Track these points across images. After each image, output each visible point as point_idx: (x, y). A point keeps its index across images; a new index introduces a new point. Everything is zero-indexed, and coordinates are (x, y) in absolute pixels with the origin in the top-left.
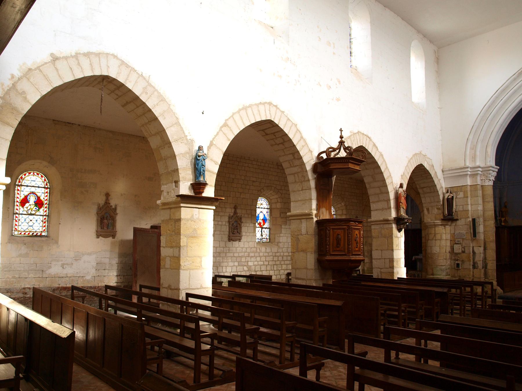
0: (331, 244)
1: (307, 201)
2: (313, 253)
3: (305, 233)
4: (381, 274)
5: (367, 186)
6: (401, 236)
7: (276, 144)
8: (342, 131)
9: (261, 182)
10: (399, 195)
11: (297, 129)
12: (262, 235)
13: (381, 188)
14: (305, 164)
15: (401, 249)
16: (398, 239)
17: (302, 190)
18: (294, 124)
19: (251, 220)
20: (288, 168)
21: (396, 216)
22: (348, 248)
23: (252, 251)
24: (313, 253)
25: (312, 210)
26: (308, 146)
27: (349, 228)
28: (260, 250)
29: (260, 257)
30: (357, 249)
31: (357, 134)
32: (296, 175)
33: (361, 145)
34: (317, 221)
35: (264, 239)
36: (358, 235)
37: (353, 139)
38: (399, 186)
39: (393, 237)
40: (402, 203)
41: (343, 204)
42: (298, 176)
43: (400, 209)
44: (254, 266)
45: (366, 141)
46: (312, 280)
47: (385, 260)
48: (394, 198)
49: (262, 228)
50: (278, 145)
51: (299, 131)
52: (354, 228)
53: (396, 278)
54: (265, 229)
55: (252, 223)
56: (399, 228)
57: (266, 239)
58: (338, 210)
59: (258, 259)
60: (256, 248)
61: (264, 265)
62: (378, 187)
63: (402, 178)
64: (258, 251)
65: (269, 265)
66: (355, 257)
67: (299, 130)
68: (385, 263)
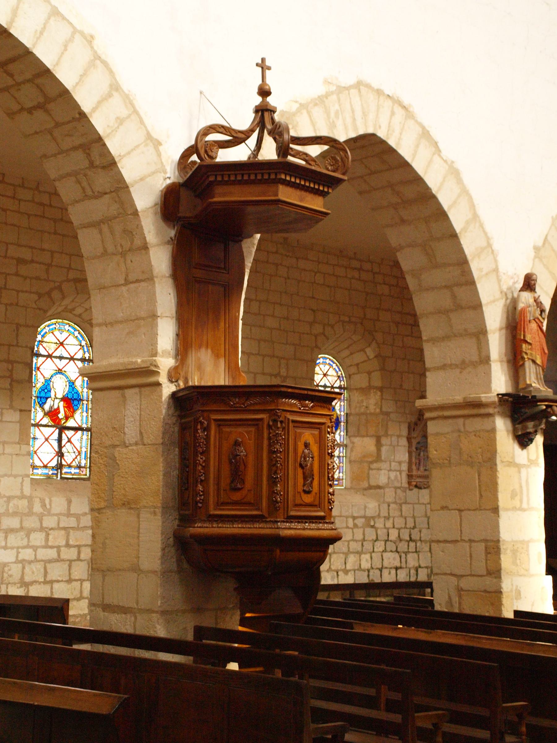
0: (212, 476)
1: (142, 322)
2: (157, 510)
3: (133, 441)
4: (460, 596)
5: (411, 282)
6: (529, 460)
7: (22, 109)
8: (269, 68)
9: (49, 265)
10: (520, 316)
11: (95, 52)
12: (60, 454)
13: (455, 289)
14: (127, 187)
15: (530, 509)
16: (519, 472)
17: (127, 282)
18: (82, 33)
19: (11, 400)
20: (77, 202)
21: (510, 390)
22: (272, 493)
23: (11, 511)
24: (157, 510)
25: (155, 354)
26: (142, 122)
27: (275, 421)
28: (44, 505)
29: (47, 531)
30: (307, 499)
31: (353, 91)
32: (105, 228)
33: (370, 131)
34: (174, 395)
35: (70, 466)
36: (315, 448)
37: (337, 107)
38: (520, 285)
39: (496, 465)
40: (530, 344)
41: (370, 352)
42: (112, 232)
43: (523, 365)
44: (20, 565)
45: (391, 118)
46: (153, 612)
47: (473, 544)
48: (504, 325)
49: (62, 429)
50: (30, 111)
51: (105, 64)
52: (293, 421)
53: (509, 614)
54: (72, 432)
55: (15, 410)
56: (520, 433)
57: (79, 467)
58: (354, 374)
59: (38, 538)
60: (30, 499)
61: (59, 560)
62: (446, 287)
63: (535, 257)
64: (37, 508)
65: (79, 559)
66: (300, 526)
67: (103, 57)
68: (471, 556)
